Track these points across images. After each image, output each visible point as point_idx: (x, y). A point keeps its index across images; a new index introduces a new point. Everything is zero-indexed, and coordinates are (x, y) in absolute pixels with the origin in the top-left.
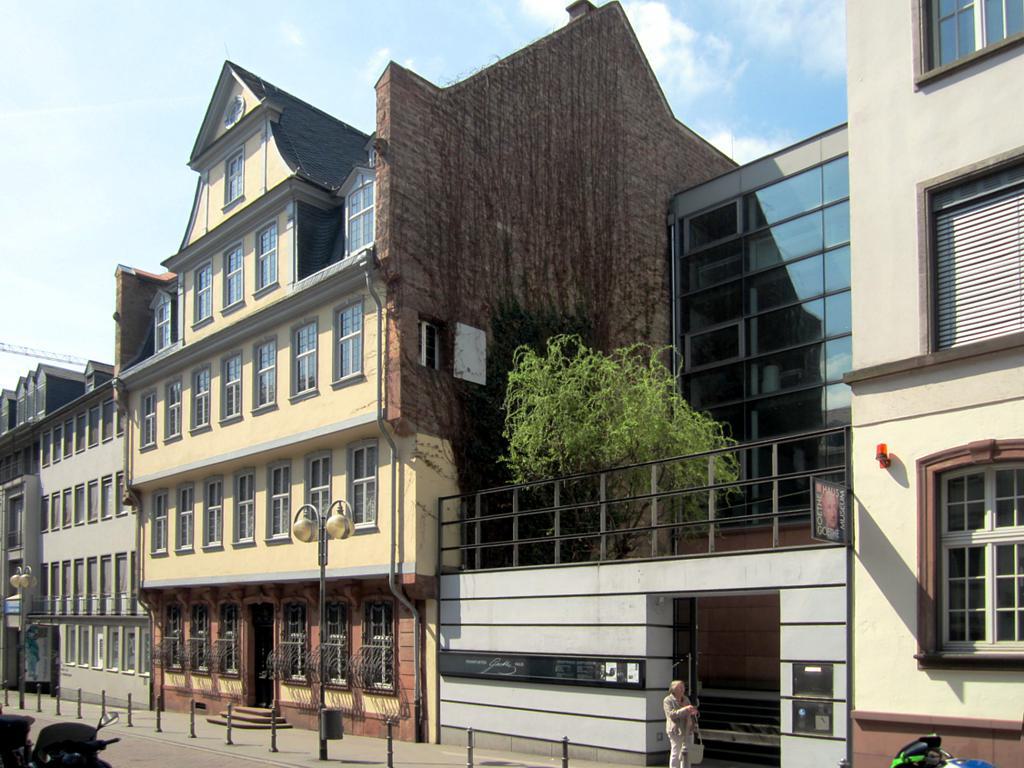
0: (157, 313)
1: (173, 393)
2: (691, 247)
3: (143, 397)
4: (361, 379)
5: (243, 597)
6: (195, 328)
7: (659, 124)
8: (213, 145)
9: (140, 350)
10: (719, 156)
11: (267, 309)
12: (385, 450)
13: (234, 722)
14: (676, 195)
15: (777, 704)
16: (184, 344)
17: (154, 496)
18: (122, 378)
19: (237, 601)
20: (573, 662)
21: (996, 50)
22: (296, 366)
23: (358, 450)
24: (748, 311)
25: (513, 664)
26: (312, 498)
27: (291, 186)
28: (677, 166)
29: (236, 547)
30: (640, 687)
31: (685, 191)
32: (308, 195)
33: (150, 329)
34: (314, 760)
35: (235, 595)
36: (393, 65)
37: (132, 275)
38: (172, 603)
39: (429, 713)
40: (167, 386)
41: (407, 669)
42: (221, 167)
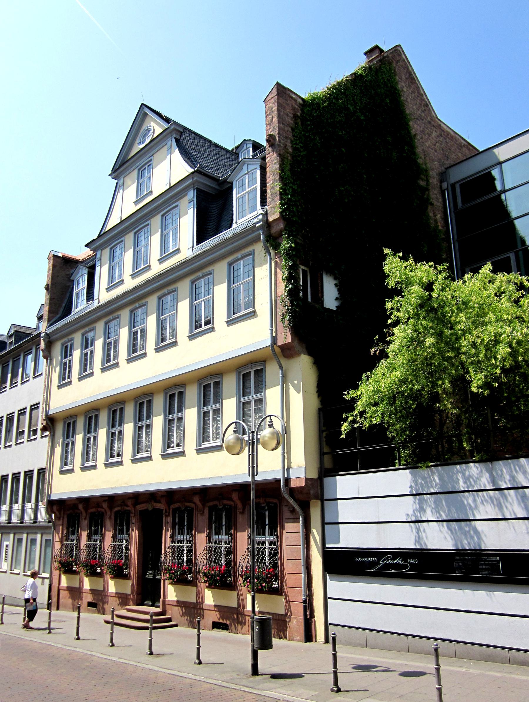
0: (76, 282)
1: (87, 340)
2: (463, 203)
3: (63, 345)
4: (253, 314)
5: (135, 505)
6: (108, 289)
9: (61, 310)
10: (466, 143)
11: (171, 269)
12: (272, 371)
13: (117, 620)
14: (446, 169)
16: (99, 303)
17: (65, 423)
18: (48, 332)
19: (130, 508)
22: (194, 310)
23: (250, 373)
24: (516, 247)
25: (405, 560)
26: (243, 410)
27: (193, 178)
28: (442, 150)
29: (134, 461)
32: (206, 185)
33: (68, 295)
35: (130, 503)
36: (278, 84)
38: (72, 513)
39: (316, 614)
40: (83, 335)
41: (291, 567)
42: (135, 173)
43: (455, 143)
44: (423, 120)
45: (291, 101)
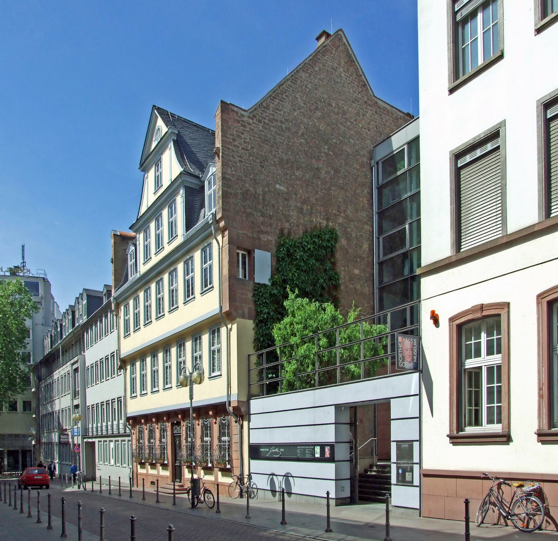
7: (366, 102)
8: (150, 155)
15: (390, 466)
20: (304, 447)
21: (491, 62)
23: (212, 325)
28: (376, 127)
30: (331, 459)
31: (381, 143)
34: (189, 508)
37: (118, 235)
43: (391, 117)
44: (358, 102)
45: (233, 114)
